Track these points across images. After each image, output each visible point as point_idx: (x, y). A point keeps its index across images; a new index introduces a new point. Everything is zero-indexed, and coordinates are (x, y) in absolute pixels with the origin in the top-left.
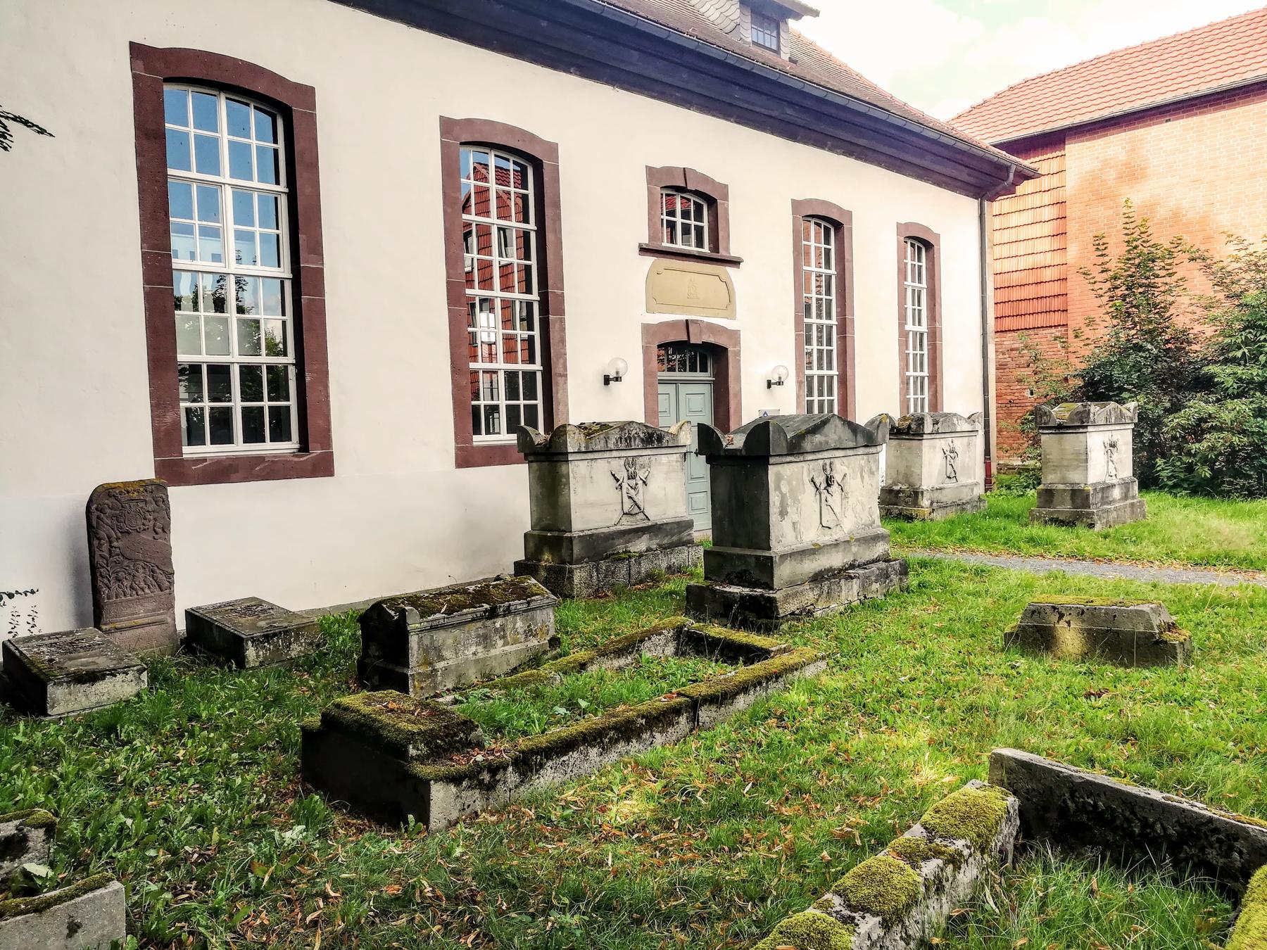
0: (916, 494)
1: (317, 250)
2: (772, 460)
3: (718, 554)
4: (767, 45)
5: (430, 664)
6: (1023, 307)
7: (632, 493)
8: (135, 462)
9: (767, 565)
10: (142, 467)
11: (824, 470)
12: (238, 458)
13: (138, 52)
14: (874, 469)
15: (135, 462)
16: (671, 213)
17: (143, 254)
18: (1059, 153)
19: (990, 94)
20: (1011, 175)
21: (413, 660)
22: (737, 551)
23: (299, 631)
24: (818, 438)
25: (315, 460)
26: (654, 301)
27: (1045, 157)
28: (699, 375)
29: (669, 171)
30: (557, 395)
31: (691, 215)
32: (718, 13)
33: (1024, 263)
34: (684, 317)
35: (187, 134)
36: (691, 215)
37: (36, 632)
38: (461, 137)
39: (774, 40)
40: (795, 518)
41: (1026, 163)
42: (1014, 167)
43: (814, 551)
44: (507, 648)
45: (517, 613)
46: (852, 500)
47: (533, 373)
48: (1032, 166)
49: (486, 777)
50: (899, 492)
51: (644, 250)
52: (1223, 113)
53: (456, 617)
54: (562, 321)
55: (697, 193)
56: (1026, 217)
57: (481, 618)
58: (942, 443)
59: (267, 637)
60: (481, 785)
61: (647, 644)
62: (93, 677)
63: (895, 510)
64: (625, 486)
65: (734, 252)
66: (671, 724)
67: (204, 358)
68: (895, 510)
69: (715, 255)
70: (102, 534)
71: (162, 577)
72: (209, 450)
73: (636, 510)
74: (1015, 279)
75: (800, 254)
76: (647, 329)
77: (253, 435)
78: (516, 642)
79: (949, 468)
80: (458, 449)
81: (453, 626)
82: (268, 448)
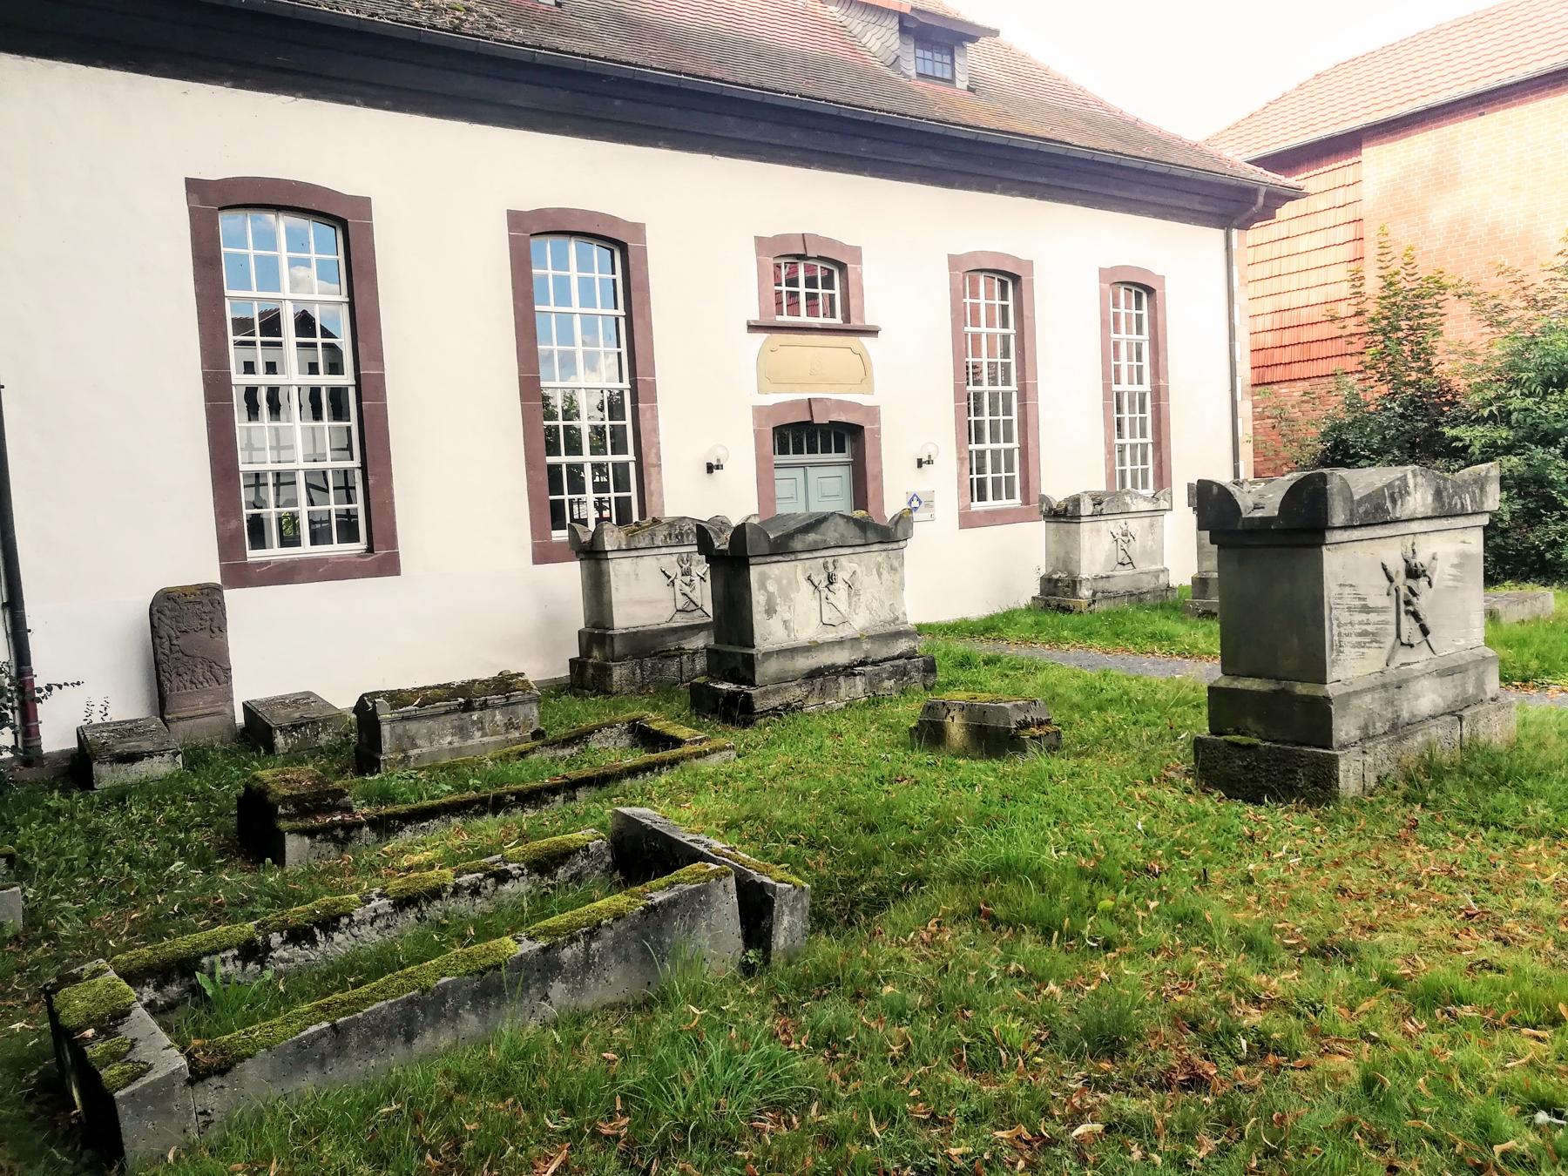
0: (1074, 584)
1: (378, 357)
2: (752, 561)
3: (716, 652)
4: (938, 75)
5: (404, 751)
6: (1316, 350)
7: (687, 589)
8: (200, 564)
9: (749, 662)
10: (209, 571)
11: (825, 567)
12: (301, 561)
13: (193, 186)
14: (896, 564)
15: (200, 564)
16: (793, 282)
17: (205, 374)
18: (1355, 159)
19: (1289, 85)
20: (1261, 200)
21: (386, 747)
22: (730, 649)
23: (326, 722)
24: (811, 537)
25: (382, 559)
26: (767, 380)
27: (1340, 164)
28: (834, 457)
29: (783, 239)
30: (651, 486)
31: (811, 284)
32: (879, 44)
33: (1316, 296)
34: (806, 396)
35: (247, 256)
36: (811, 284)
37: (107, 719)
38: (533, 230)
39: (948, 68)
40: (787, 616)
41: (1291, 181)
42: (1263, 191)
43: (812, 647)
44: (485, 739)
45: (495, 707)
46: (864, 597)
47: (626, 464)
48: (1301, 184)
49: (340, 833)
50: (1058, 580)
51: (753, 328)
52: (1531, 106)
53: (428, 709)
54: (654, 410)
55: (820, 258)
56: (1318, 240)
57: (456, 711)
58: (1110, 526)
59: (295, 727)
60: (335, 839)
61: (597, 736)
62: (133, 758)
63: (1053, 601)
64: (677, 582)
65: (869, 321)
66: (546, 802)
67: (269, 466)
68: (1053, 601)
69: (847, 326)
70: (163, 633)
71: (220, 673)
72: (275, 552)
73: (692, 607)
74: (1305, 316)
75: (960, 316)
76: (759, 411)
77: (289, 540)
78: (495, 733)
79: (1122, 554)
80: (535, 546)
81: (426, 717)
82: (1004, 503)
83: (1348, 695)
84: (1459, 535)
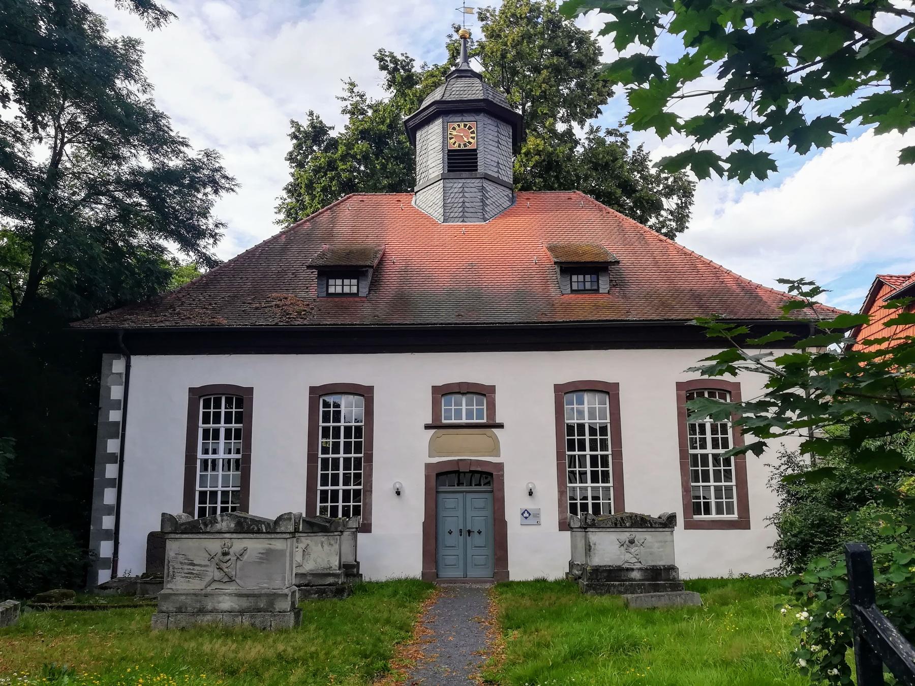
51: (427, 427)
65: (498, 420)
76: (428, 466)
83: (171, 594)
84: (267, 541)
